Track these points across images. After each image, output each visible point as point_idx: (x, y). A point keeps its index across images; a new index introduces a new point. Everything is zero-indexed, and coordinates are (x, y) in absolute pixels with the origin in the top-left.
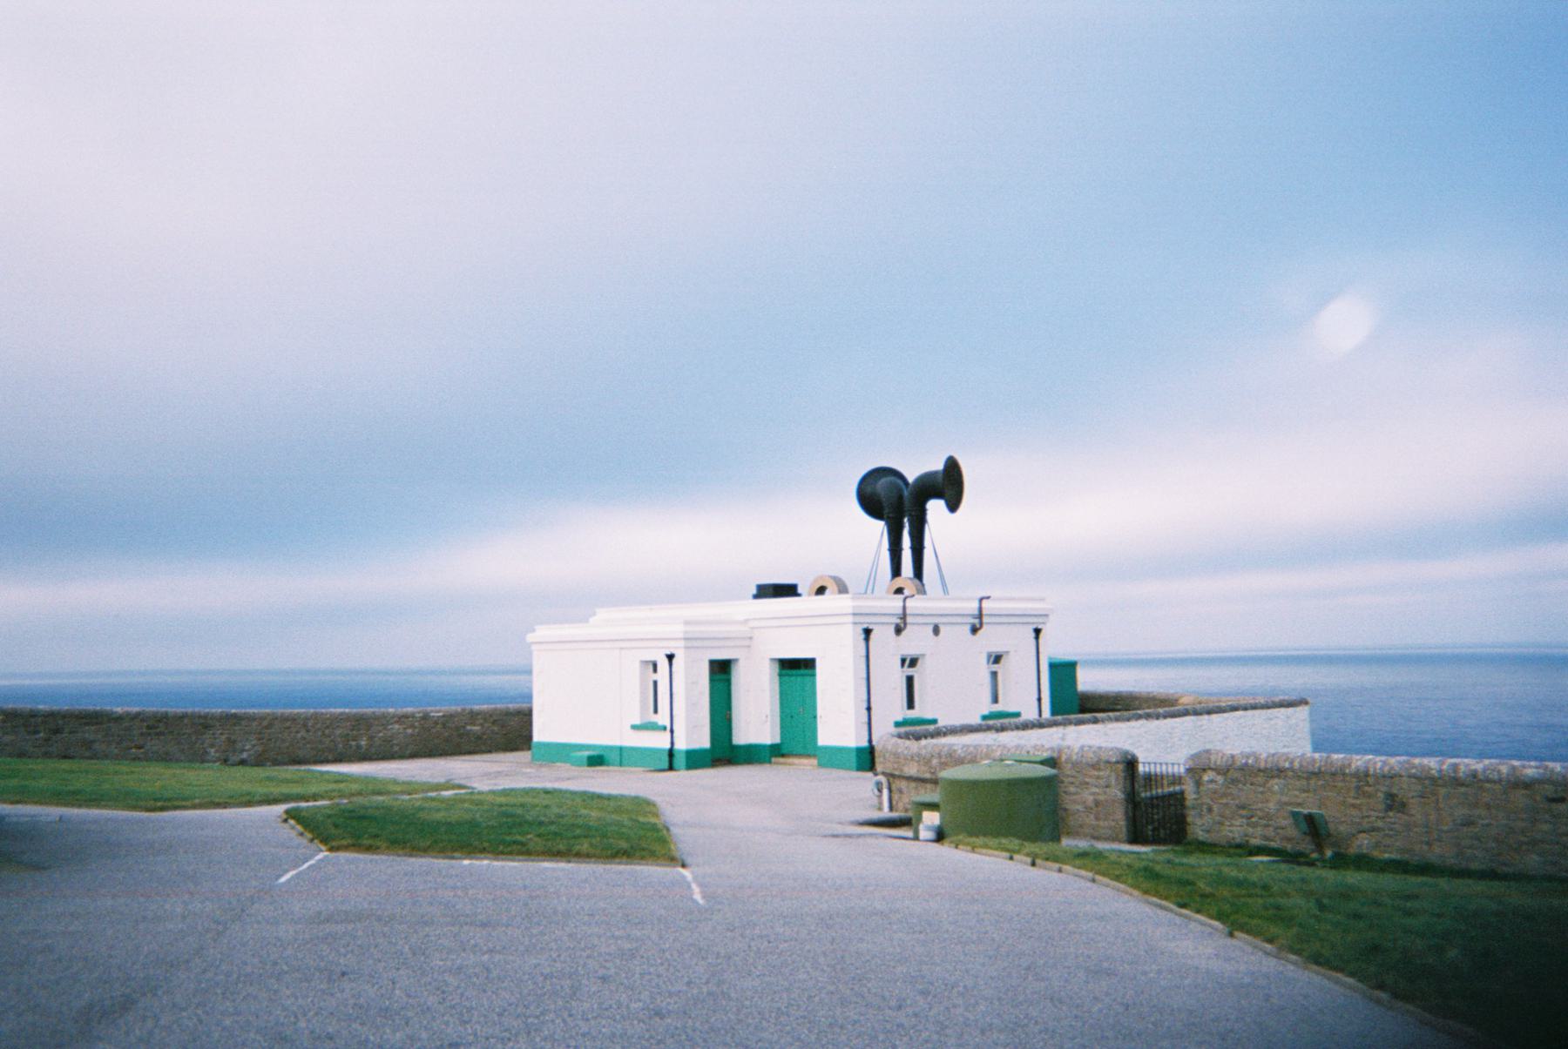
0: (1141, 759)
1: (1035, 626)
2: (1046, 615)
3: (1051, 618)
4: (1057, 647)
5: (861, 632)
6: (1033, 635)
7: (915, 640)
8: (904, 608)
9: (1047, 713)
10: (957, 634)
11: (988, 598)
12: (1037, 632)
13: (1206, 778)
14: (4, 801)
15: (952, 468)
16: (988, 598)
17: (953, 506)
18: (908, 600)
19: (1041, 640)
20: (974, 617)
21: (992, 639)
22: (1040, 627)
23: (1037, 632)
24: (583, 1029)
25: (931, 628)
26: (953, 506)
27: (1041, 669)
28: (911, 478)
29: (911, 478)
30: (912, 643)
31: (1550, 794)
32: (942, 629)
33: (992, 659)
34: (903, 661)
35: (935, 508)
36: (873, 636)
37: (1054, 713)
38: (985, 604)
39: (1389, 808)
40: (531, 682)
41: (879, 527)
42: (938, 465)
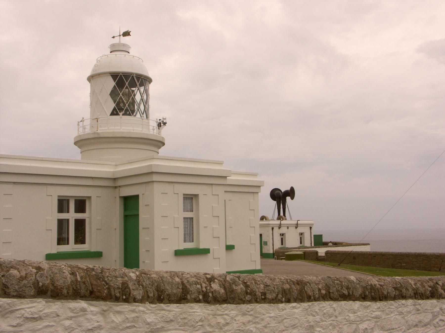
0: (319, 252)
1: (272, 227)
2: (313, 224)
3: (314, 225)
4: (315, 232)
5: (271, 228)
6: (310, 229)
7: (283, 230)
8: (281, 223)
9: (313, 245)
10: (292, 229)
11: (299, 220)
12: (311, 228)
13: (328, 255)
14: (0, 298)
15: (292, 189)
16: (299, 220)
17: (292, 198)
18: (281, 221)
19: (274, 230)
20: (296, 225)
21: (300, 230)
22: (311, 227)
23: (311, 228)
24: (205, 281)
25: (286, 227)
26: (292, 198)
27: (312, 236)
28: (283, 191)
29: (283, 191)
30: (283, 230)
31: (374, 256)
32: (289, 227)
33: (300, 234)
34: (280, 234)
35: (288, 198)
36: (274, 229)
37: (314, 245)
38: (299, 222)
39: (354, 259)
40: (66, 213)
41: (275, 202)
42: (289, 189)
